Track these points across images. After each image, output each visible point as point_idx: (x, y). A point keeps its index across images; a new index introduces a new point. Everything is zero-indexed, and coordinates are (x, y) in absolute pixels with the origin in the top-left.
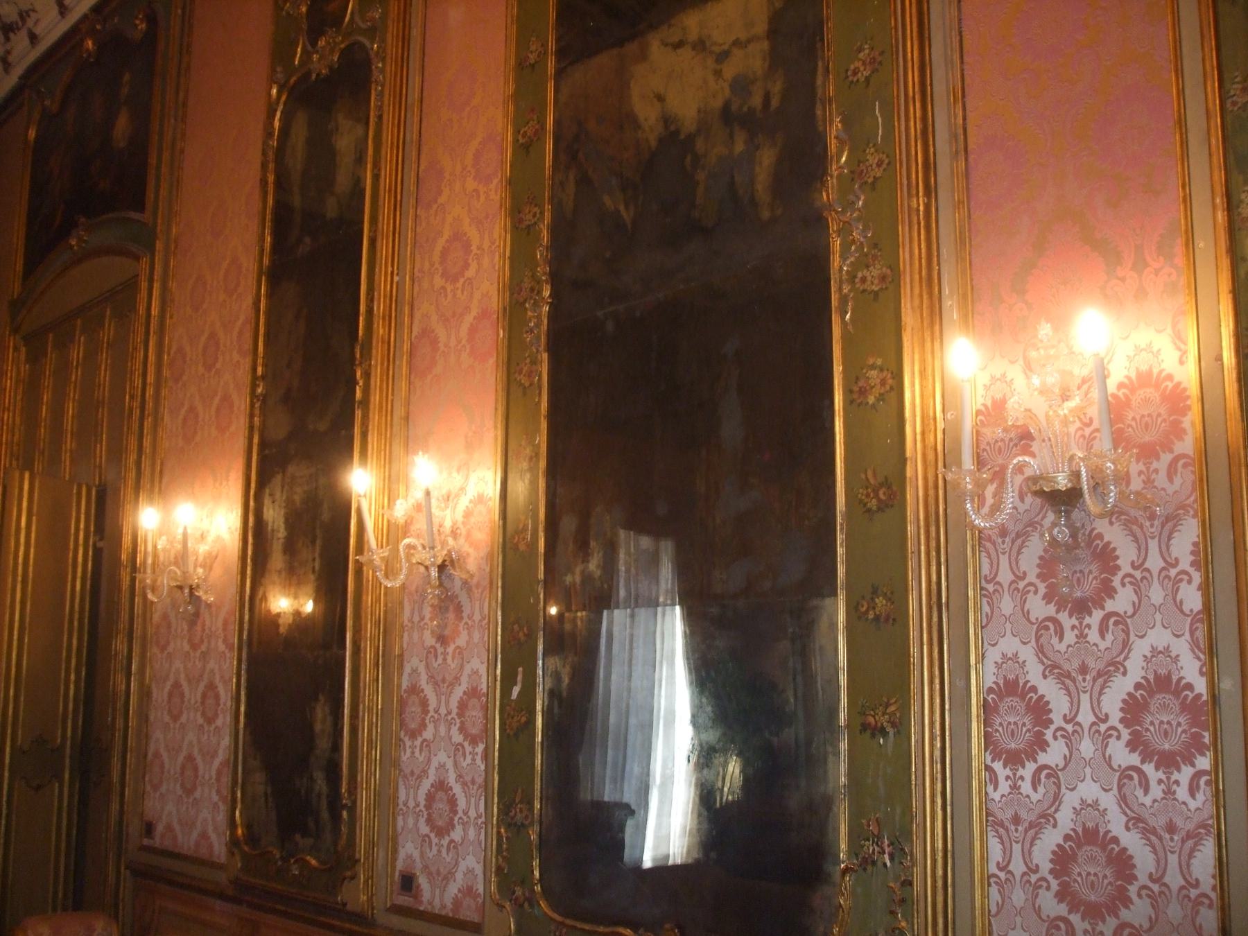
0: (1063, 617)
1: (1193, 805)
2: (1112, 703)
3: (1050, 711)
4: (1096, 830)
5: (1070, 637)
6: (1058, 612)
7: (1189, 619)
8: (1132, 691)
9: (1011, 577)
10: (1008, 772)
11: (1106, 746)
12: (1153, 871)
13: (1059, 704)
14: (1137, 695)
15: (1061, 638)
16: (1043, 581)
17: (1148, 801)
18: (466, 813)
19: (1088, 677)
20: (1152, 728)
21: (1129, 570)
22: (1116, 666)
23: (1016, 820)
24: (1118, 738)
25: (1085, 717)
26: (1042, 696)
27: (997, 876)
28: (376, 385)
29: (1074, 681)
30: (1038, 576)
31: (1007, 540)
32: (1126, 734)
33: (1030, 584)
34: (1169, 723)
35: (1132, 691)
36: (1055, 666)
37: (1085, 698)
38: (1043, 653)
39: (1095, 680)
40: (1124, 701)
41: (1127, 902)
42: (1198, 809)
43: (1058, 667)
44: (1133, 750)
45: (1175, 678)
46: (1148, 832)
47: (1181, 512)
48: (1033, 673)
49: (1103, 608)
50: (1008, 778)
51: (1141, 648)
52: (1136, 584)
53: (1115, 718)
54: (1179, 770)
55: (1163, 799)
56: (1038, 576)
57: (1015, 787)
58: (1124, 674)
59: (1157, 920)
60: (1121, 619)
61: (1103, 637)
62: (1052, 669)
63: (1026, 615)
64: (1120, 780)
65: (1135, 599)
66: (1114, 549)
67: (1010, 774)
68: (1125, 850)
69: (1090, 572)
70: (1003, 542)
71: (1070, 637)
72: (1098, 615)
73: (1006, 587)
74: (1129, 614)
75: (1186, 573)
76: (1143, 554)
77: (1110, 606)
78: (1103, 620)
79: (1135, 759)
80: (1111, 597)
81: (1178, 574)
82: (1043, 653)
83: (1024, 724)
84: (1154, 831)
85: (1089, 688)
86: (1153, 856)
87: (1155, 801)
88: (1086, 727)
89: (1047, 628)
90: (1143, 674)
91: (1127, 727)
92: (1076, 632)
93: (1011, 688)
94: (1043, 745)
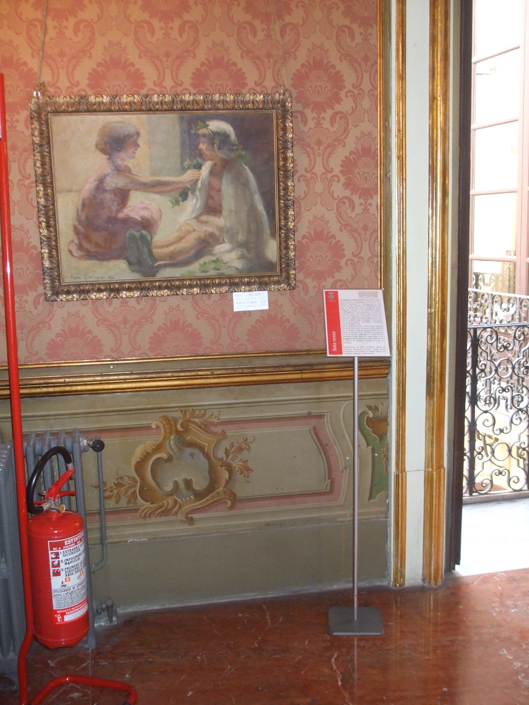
0: (355, 198)
1: (332, 130)
2: (336, 163)
3: (246, 78)
4: (322, 232)
5: (359, 209)
6: (352, 194)
7: (337, 201)
8: (348, 155)
12: (355, 251)
14: (351, 158)
15: (353, 210)
16: (295, 89)
17: (353, 215)
19: (321, 148)
21: (351, 88)
22: (340, 141)
24: (338, 181)
26: (339, 72)
29: (359, 234)
30: (341, 172)
31: (368, 233)
32: (343, 180)
34: (320, 86)
35: (348, 155)
36: (348, 225)
38: (341, 217)
39: (325, 149)
40: (343, 161)
42: (335, 132)
44: (347, 188)
46: (353, 232)
48: (334, 227)
51: (354, 132)
52: (354, 96)
53: (337, 170)
54: (325, 112)
55: (362, 213)
56: (341, 172)
58: (344, 146)
59: (308, 192)
60: (344, 116)
61: (332, 125)
62: (345, 226)
64: (338, 204)
68: (239, 70)
69: (326, 87)
70: (366, 234)
71: (359, 209)
72: (329, 113)
74: (349, 113)
80: (339, 103)
82: (341, 217)
84: (356, 231)
85: (368, 238)
86: (355, 243)
87: (310, 129)
88: (319, 175)
90: (355, 146)
92: (315, 121)
93: (319, 235)
94: (339, 269)
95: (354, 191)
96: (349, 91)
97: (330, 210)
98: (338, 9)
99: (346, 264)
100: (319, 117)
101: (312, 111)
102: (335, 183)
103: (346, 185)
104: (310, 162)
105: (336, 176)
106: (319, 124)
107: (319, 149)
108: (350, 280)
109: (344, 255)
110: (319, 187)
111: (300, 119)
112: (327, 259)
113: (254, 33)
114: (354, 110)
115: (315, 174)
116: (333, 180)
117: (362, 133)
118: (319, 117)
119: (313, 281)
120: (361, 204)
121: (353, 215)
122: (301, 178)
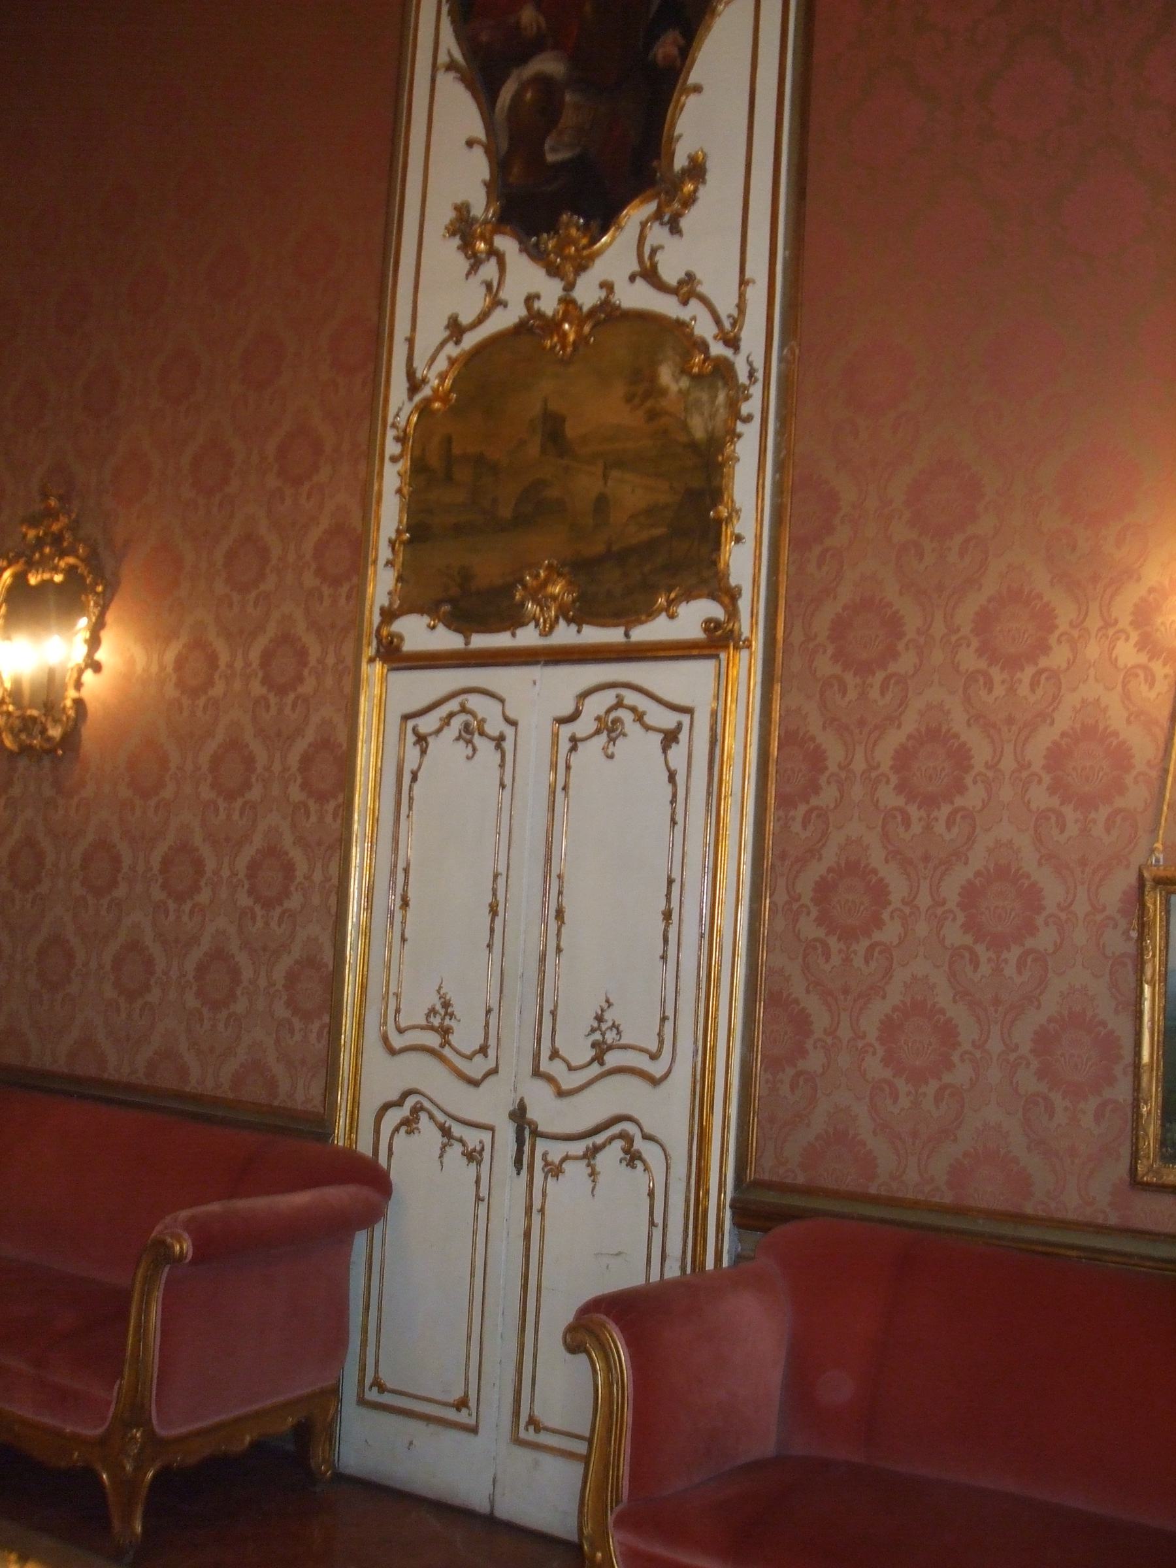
9: (786, 898)
10: (842, 946)
11: (942, 927)
14: (977, 882)
17: (1152, 695)
18: (268, 769)
26: (882, 880)
27: (901, 911)
33: (883, 774)
41: (950, 1066)
45: (1101, 727)
47: (954, 858)
49: (952, 803)
53: (873, 1034)
56: (812, 900)
66: (970, 750)
69: (943, 769)
73: (780, 909)
75: (871, 1045)
76: (1081, 617)
77: (877, 936)
78: (951, 813)
79: (887, 1074)
89: (815, 948)
96: (980, 774)
97: (938, 967)
100: (928, 816)
101: (1002, 669)
102: (1121, 644)
103: (966, 928)
104: (995, 751)
105: (951, 911)
106: (1012, 690)
107: (846, 999)
108: (1051, 950)
110: (922, 929)
112: (1013, 914)
113: (921, 556)
116: (866, 1052)
118: (928, 816)
119: (1165, 664)
120: (908, 1094)
121: (1152, 695)
122: (1063, 638)
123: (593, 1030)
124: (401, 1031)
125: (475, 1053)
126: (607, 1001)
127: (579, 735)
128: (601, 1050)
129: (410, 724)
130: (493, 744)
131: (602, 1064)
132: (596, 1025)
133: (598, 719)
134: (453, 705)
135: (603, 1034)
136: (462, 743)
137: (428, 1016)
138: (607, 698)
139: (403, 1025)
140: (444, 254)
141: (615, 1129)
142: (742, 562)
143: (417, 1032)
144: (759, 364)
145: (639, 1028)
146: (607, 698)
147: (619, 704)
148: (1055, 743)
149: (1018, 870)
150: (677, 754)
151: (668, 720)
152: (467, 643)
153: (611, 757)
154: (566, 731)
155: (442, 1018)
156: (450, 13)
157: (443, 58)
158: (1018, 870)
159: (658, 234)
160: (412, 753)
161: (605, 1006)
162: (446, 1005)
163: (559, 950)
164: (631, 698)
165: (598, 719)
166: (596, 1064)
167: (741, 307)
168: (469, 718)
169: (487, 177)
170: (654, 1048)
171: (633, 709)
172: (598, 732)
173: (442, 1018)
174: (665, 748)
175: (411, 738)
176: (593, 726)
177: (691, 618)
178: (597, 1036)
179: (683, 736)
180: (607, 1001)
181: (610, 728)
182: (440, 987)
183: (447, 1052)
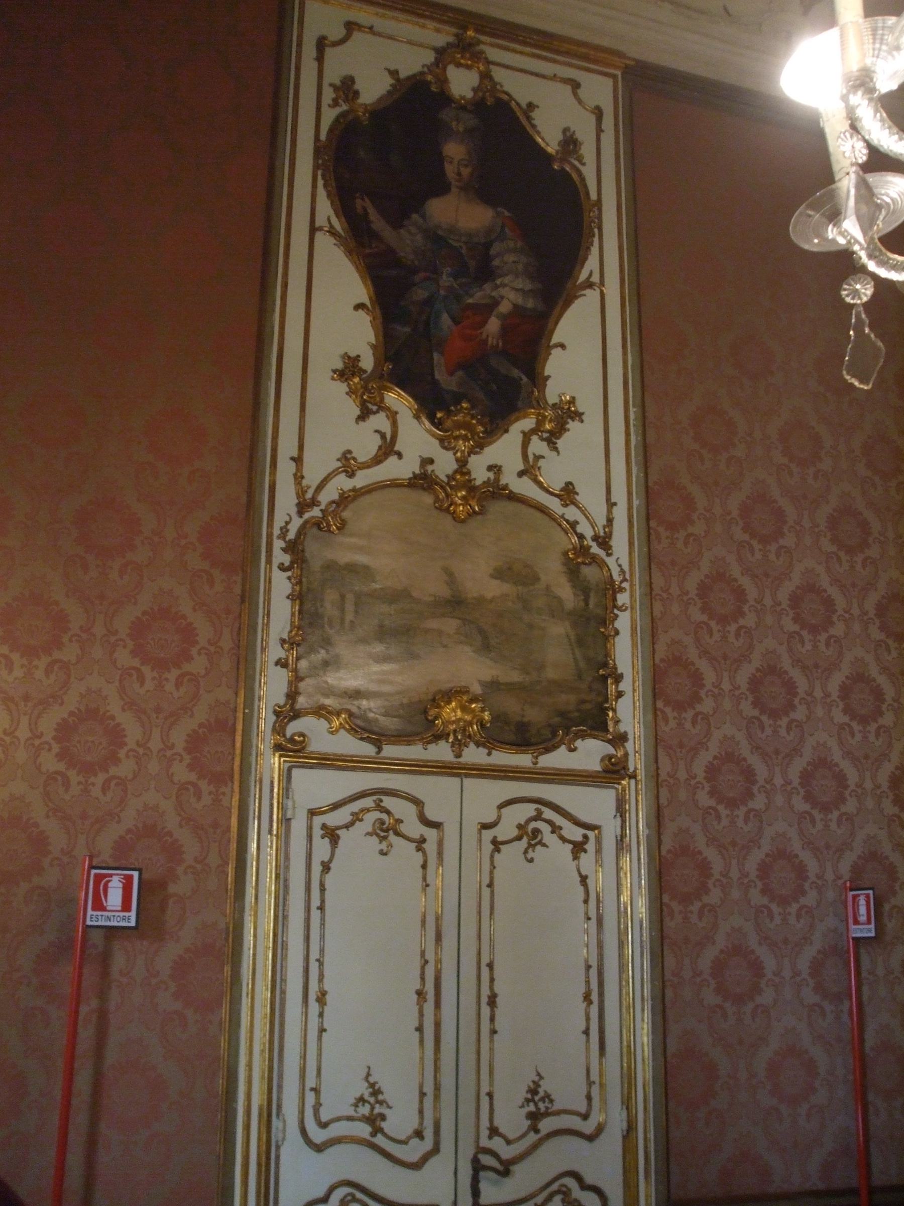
2: (794, 773)
7: (120, 672)
13: (761, 771)
15: (67, 790)
20: (78, 745)
22: (796, 751)
23: (84, 816)
25: (818, 693)
28: (731, 78)
34: (93, 742)
37: (868, 774)
43: (761, 748)
50: (821, 820)
53: (796, 782)
57: (827, 826)
63: (832, 719)
64: (121, 676)
65: (766, 801)
67: (214, 790)
79: (61, 767)
80: (844, 804)
81: (117, 640)
83: (101, 743)
88: (778, 786)
89: (56, 780)
91: (803, 787)
94: (707, 891)
95: (853, 717)
98: (746, 699)
99: (199, 654)
109: (704, 685)
111: (135, 677)
114: (808, 718)
115: (17, 737)
117: (725, 736)
119: (78, 775)
123: (528, 1101)
124: (324, 1125)
125: (410, 1138)
126: (538, 1074)
127: (500, 839)
128: (535, 1117)
129: (318, 821)
130: (413, 846)
131: (537, 1131)
132: (529, 1096)
133: (520, 827)
134: (368, 802)
135: (536, 1104)
136: (375, 839)
137: (356, 1105)
138: (530, 810)
139: (324, 1118)
140: (333, 401)
141: (555, 1187)
142: (629, 712)
143: (344, 1123)
144: (626, 567)
145: (566, 1090)
146: (530, 810)
147: (538, 817)
148: (121, 837)
149: (163, 828)
150: (587, 860)
151: (576, 834)
152: (379, 752)
153: (531, 861)
154: (488, 835)
155: (372, 1109)
156: (325, 186)
157: (320, 221)
158: (163, 828)
159: (537, 446)
160: (322, 848)
161: (536, 1079)
162: (376, 1092)
163: (494, 1032)
164: (548, 814)
165: (520, 827)
166: (532, 1134)
167: (610, 521)
168: (384, 816)
169: (373, 340)
170: (583, 1109)
171: (549, 822)
172: (519, 838)
173: (372, 1109)
174: (576, 858)
175: (317, 832)
176: (515, 832)
177: (589, 753)
178: (532, 1108)
179: (591, 846)
180: (538, 1074)
181: (530, 836)
182: (368, 1075)
183: (379, 1140)
